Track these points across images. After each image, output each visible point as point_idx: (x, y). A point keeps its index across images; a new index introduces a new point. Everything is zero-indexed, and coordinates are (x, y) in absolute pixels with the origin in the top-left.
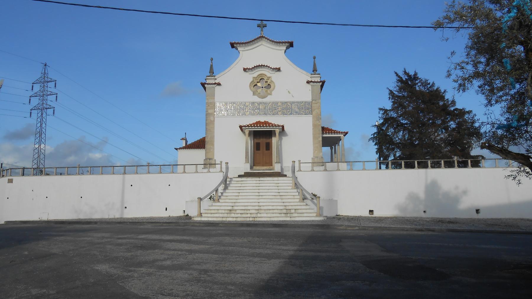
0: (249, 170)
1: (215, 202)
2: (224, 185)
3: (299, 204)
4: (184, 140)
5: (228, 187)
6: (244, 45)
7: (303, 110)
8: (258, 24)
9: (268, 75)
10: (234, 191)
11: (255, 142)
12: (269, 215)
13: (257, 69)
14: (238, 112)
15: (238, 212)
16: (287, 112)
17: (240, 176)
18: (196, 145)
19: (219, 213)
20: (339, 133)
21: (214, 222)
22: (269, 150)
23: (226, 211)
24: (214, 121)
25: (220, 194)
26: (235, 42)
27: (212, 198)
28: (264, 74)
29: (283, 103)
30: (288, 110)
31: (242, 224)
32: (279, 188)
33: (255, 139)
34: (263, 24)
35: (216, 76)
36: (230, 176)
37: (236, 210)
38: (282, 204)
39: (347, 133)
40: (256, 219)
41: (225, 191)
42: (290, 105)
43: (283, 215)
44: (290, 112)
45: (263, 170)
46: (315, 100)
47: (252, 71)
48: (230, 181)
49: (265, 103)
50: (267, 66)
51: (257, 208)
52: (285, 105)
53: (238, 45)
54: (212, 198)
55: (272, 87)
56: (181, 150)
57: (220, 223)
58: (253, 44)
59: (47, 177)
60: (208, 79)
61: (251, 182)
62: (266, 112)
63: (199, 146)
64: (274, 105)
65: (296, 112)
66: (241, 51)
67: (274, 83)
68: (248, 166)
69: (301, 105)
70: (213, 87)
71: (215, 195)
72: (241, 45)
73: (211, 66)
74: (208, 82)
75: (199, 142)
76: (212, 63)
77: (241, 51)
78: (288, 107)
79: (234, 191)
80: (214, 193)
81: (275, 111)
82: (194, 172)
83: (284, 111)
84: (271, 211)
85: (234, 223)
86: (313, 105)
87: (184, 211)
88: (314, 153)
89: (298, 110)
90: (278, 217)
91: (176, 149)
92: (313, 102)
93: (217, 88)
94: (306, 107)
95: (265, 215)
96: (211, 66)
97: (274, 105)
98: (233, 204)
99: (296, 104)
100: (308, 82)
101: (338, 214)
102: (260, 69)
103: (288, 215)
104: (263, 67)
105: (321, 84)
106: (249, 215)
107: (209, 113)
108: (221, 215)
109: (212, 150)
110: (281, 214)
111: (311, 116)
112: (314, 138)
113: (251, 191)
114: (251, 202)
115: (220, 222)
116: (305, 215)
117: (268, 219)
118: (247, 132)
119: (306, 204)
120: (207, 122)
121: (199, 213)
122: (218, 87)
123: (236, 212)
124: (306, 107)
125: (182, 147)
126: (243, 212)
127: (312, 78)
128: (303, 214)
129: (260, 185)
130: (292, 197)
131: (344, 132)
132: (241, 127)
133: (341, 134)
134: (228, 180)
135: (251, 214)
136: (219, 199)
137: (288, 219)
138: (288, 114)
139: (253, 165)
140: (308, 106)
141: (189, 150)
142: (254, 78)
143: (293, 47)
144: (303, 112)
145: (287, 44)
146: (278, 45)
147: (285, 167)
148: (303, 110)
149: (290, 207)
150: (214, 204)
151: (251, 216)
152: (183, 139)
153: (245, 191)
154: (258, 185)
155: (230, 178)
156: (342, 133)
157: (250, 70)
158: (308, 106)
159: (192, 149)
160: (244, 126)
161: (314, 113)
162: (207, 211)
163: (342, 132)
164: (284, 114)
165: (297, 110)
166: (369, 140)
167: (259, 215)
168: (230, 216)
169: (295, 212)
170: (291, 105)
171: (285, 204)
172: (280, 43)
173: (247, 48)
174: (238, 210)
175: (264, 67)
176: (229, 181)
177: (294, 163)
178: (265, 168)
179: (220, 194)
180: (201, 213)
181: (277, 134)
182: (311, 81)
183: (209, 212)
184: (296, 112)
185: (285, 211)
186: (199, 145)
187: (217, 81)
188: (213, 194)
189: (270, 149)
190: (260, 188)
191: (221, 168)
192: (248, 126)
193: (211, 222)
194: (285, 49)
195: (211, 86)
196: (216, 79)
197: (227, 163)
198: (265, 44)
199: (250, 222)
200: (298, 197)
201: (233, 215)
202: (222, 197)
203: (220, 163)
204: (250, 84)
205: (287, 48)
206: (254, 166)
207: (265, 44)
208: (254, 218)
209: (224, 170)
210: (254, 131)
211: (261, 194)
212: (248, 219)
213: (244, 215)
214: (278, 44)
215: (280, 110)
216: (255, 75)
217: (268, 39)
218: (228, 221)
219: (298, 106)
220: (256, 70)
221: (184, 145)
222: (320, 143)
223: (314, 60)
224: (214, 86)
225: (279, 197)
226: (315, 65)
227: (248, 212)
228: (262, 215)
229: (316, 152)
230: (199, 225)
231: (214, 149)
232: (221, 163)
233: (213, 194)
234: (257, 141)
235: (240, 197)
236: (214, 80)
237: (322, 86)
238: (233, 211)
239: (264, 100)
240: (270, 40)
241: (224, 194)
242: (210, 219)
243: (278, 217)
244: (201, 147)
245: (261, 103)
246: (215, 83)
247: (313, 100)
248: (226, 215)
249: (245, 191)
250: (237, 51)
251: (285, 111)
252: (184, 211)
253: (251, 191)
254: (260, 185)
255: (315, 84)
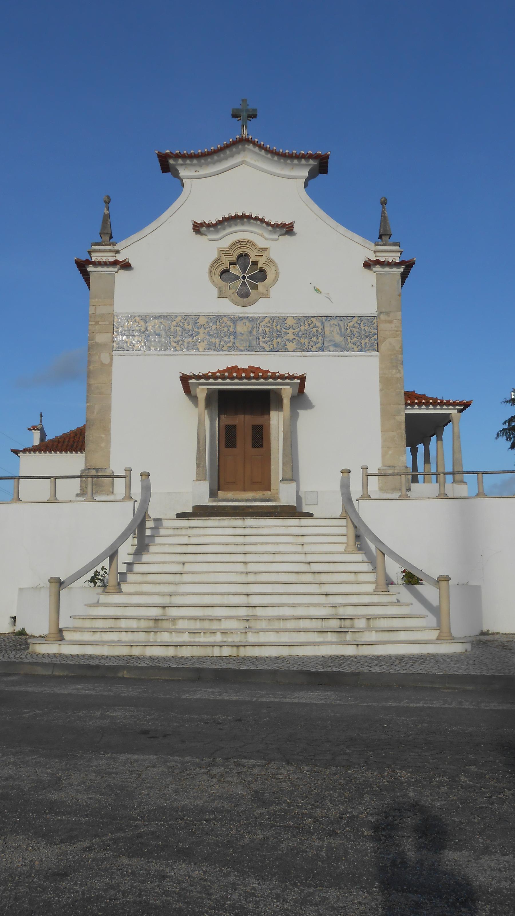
0: (206, 501)
1: (109, 594)
2: (136, 540)
3: (376, 599)
4: (38, 429)
5: (148, 545)
6: (195, 161)
7: (355, 339)
8: (233, 110)
9: (261, 243)
10: (167, 558)
11: (222, 424)
12: (285, 638)
13: (230, 226)
14: (177, 342)
15: (182, 625)
16: (311, 343)
17: (180, 515)
18: (66, 443)
19: (119, 630)
20: (448, 404)
21: (103, 662)
22: (261, 445)
23: (143, 624)
24: (111, 364)
25: (123, 568)
26: (171, 152)
27: (98, 579)
28: (249, 242)
29: (300, 320)
30: (314, 339)
31: (198, 670)
32: (307, 548)
33: (223, 417)
34: (247, 110)
35: (118, 245)
36: (153, 513)
37: (174, 620)
38: (322, 600)
39: (467, 405)
40: (243, 652)
41: (140, 560)
42: (318, 324)
43: (330, 637)
44: (319, 345)
45: (247, 500)
46: (388, 313)
47: (217, 231)
48: (155, 528)
49: (252, 319)
50: (257, 219)
51: (243, 612)
52: (307, 324)
53: (180, 161)
54: (98, 579)
55: (270, 276)
56: (28, 454)
57: (124, 668)
58: (220, 161)
59: (324, 591)
60: (95, 251)
61: (219, 531)
62: (254, 343)
63: (75, 446)
64: (274, 324)
65: (336, 345)
66: (187, 177)
67: (275, 265)
68: (205, 487)
69: (349, 324)
70: (110, 273)
71: (108, 568)
72: (188, 162)
73: (106, 219)
74: (96, 257)
75: (74, 437)
76: (108, 210)
77: (187, 177)
78: (314, 330)
79: (167, 558)
80: (106, 563)
81: (279, 340)
82: (46, 500)
83: (302, 341)
84: (291, 625)
85: (170, 668)
86: (381, 326)
87: (14, 618)
88: (384, 456)
89: (342, 338)
90: (314, 644)
91: (16, 452)
92: (382, 317)
93: (122, 275)
94: (363, 332)
95: (272, 637)
96: (106, 219)
97: (274, 324)
98: (166, 600)
99: (332, 322)
100: (368, 265)
101: (485, 630)
102: (239, 228)
103: (349, 637)
104: (245, 220)
105: (402, 270)
106: (218, 638)
107: (97, 344)
108: (125, 637)
109: (103, 445)
110: (325, 634)
111: (376, 356)
112: (385, 414)
113: (219, 558)
114: (223, 594)
115: (122, 663)
116: (402, 636)
117: (285, 652)
118: (201, 392)
119: (398, 601)
120: (91, 368)
121: (54, 630)
122: (122, 272)
123: (174, 625)
124: (363, 332)
125: (29, 446)
126: (198, 625)
127: (378, 254)
128: (395, 633)
129: (248, 540)
130: (351, 577)
131: (460, 404)
132: (185, 379)
133: (451, 407)
134: (149, 524)
135: (224, 633)
136: (119, 584)
137: (349, 651)
138: (312, 350)
139: (216, 488)
140: (366, 328)
141: (48, 454)
142: (221, 250)
143: (326, 173)
144: (354, 343)
145: (311, 162)
146: (286, 164)
147: (305, 492)
148: (355, 339)
149: (350, 611)
150: (104, 599)
151: (225, 639)
152: (34, 429)
153: (200, 558)
154: (240, 540)
155: (155, 520)
156: (454, 404)
157: (212, 229)
158: (366, 328)
159: (55, 452)
160: (198, 377)
161: (384, 347)
162: (79, 623)
163: (454, 402)
164: (302, 348)
165: (338, 339)
166: (498, 435)
167: (252, 638)
168: (156, 641)
169: (368, 625)
170: (323, 324)
171: (333, 600)
172: (291, 156)
173: (203, 172)
174: (183, 618)
175: (249, 223)
176: (151, 528)
177: (346, 474)
178: (250, 495)
179: (123, 568)
180: (61, 631)
181: (286, 402)
182: (378, 262)
183: (88, 624)
184: (336, 345)
185: (334, 624)
186: (74, 443)
187: (120, 258)
188: (103, 568)
189: (264, 445)
190: (247, 548)
191: (128, 486)
192: (206, 377)
193: (93, 663)
194: (307, 175)
195: (105, 269)
196: (118, 252)
197: (146, 475)
198: (253, 162)
199: (224, 666)
200: (371, 577)
201: (165, 637)
202: (131, 578)
203: (124, 473)
204: (212, 266)
205: (312, 175)
206: (219, 490)
207: (253, 162)
208: (235, 648)
209: (136, 491)
210: (221, 392)
211: (251, 568)
212: (216, 652)
213: (202, 639)
214: (289, 161)
215: (291, 336)
216: (226, 243)
217: (261, 147)
218: (151, 657)
219: (340, 329)
220: (228, 230)
221: (37, 442)
222: (400, 429)
223: (383, 207)
224: (111, 269)
225: (309, 578)
226: (384, 219)
227: (215, 626)
228: (262, 638)
229: (390, 452)
230: (50, 673)
231: (108, 442)
232: (127, 475)
233: (103, 568)
234: (227, 420)
235: (186, 578)
236: (113, 254)
237: (404, 276)
238: (165, 624)
239: (250, 310)
240: (267, 151)
241: (137, 568)
242: (90, 651)
243: (314, 644)
244: (79, 447)
245: (240, 318)
246: (115, 263)
247: (381, 313)
248: (141, 637)
249: (200, 558)
250: (176, 179)
251: (306, 340)
252: (14, 618)
253: (219, 558)
254: (248, 540)
255: (387, 269)
